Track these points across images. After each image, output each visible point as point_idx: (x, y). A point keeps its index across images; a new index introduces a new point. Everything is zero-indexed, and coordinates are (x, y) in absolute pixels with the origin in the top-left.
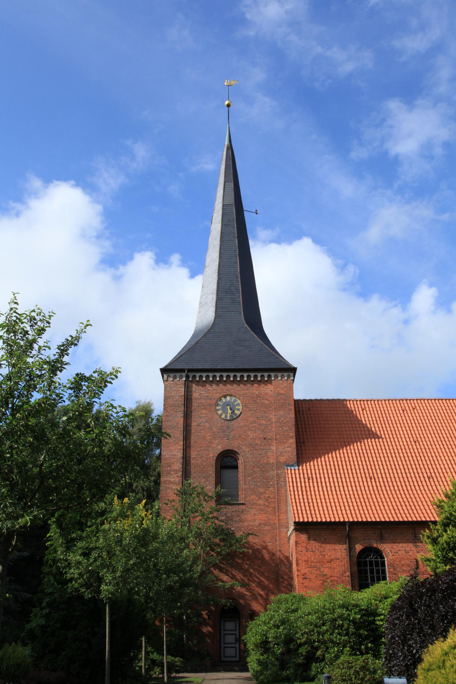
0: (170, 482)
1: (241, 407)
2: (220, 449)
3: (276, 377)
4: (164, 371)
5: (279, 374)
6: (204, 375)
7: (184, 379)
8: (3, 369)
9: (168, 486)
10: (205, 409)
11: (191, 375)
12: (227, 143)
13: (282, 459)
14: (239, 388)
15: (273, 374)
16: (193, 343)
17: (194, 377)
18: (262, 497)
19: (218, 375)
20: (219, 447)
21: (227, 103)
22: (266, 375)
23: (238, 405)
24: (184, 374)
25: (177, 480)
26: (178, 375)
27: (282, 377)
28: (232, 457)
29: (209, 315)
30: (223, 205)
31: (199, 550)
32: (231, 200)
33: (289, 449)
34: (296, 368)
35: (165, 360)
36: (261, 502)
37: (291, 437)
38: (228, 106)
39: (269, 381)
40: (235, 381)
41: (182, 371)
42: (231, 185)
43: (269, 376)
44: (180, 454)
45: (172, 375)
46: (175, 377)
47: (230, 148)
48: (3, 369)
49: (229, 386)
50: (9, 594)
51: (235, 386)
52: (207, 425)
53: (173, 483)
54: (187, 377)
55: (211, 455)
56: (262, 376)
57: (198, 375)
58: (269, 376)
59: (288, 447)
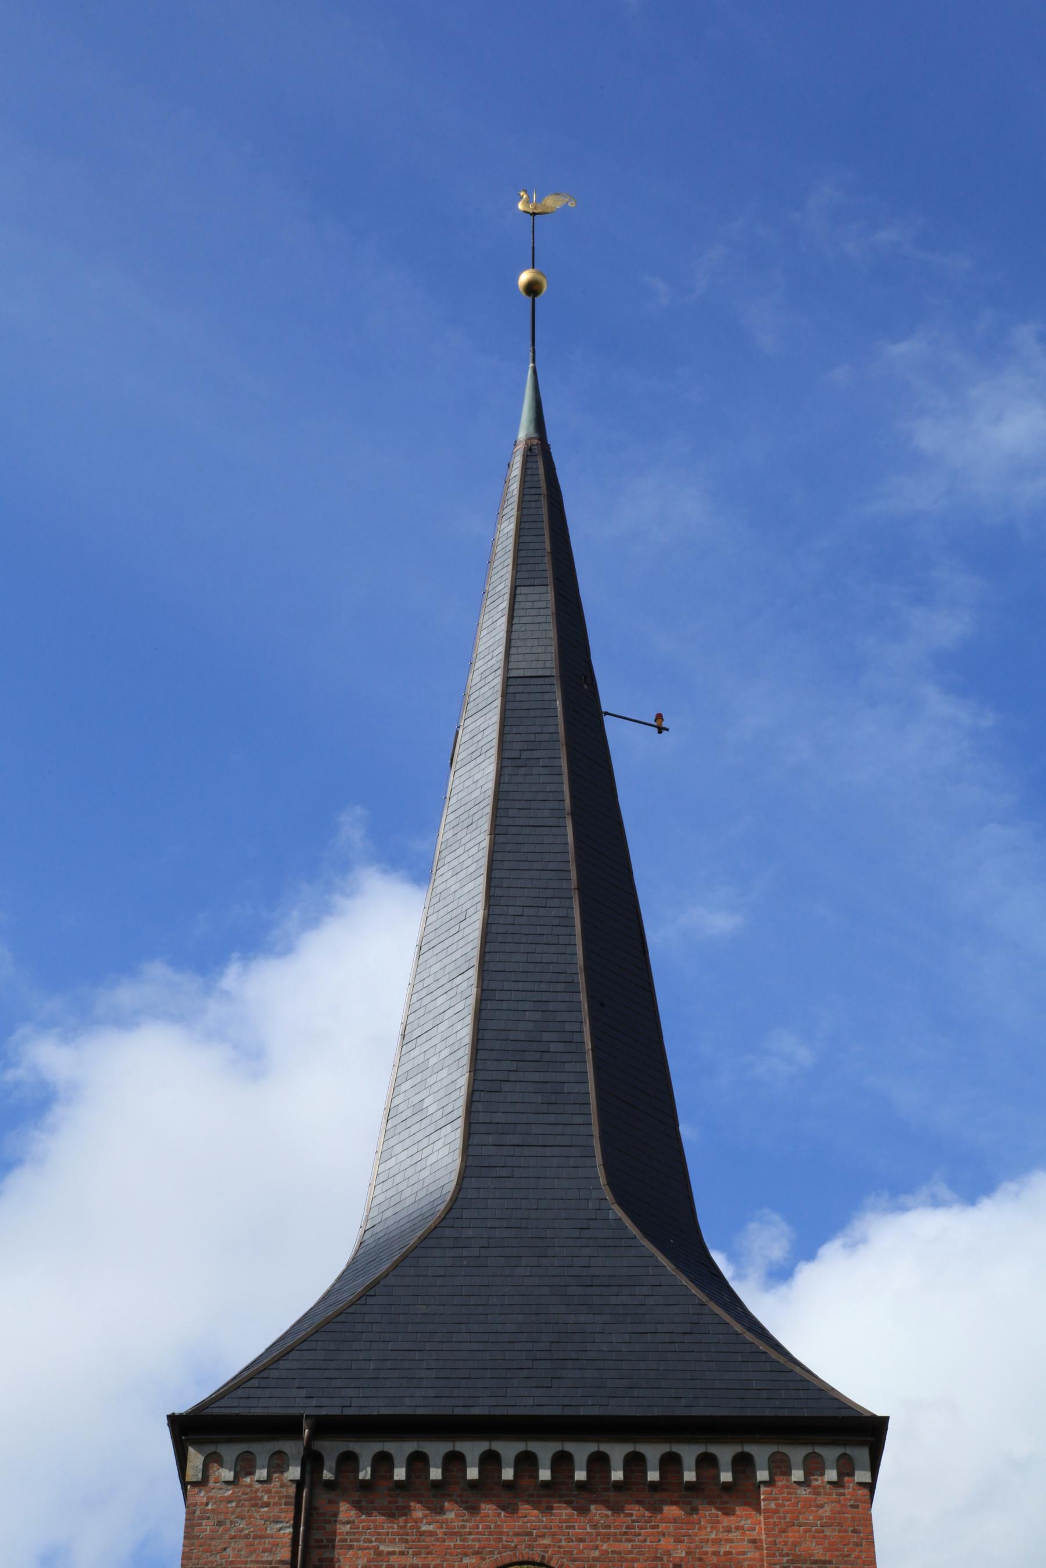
3: (780, 1466)
4: (188, 1429)
5: (797, 1454)
6: (401, 1450)
7: (294, 1472)
11: (331, 1449)
12: (524, 431)
14: (582, 1526)
15: (761, 1453)
16: (348, 1296)
17: (348, 1460)
19: (472, 1450)
21: (525, 277)
22: (725, 1453)
24: (294, 1448)
26: (262, 1450)
27: (813, 1467)
29: (437, 1159)
30: (507, 680)
32: (543, 655)
38: (532, 289)
39: (742, 1492)
40: (559, 1489)
41: (283, 1427)
42: (543, 599)
43: (743, 1464)
45: (230, 1452)
46: (245, 1466)
47: (539, 451)
49: (530, 1515)
51: (563, 1512)
54: (312, 1461)
56: (707, 1462)
57: (366, 1451)
58: (743, 1464)
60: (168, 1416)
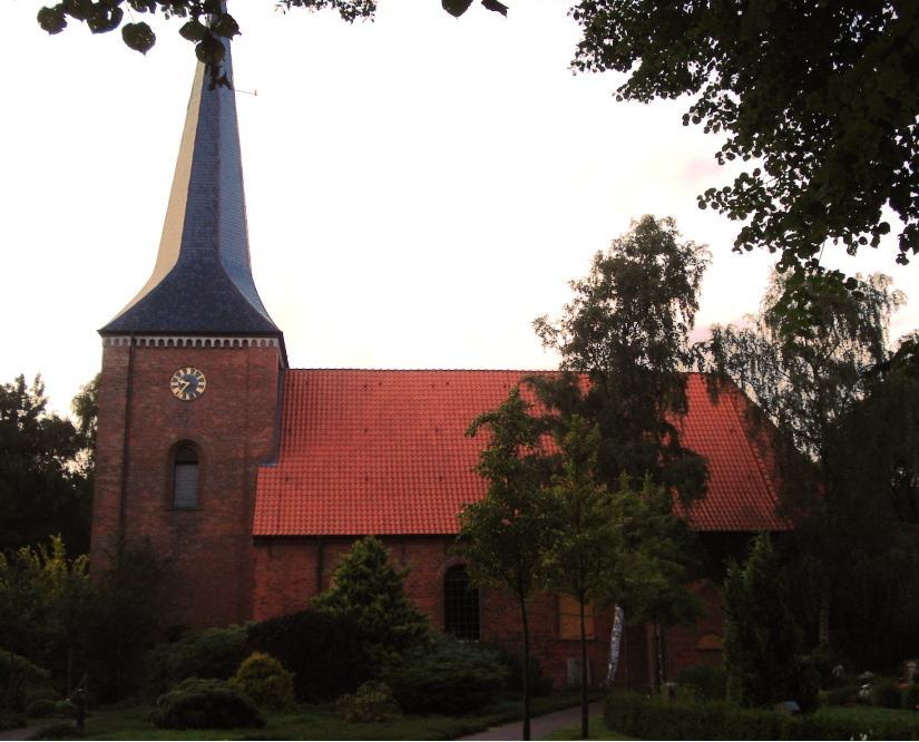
0: (106, 482)
1: (204, 384)
2: (173, 437)
4: (104, 332)
8: (116, 34)
9: (103, 486)
10: (157, 385)
13: (256, 453)
18: (226, 501)
20: (173, 436)
23: (202, 380)
25: (116, 479)
28: (191, 450)
31: (96, 592)
33: (264, 440)
34: (649, 225)
35: (106, 319)
36: (224, 508)
37: (269, 424)
44: (120, 447)
48: (116, 34)
50: (811, 72)
52: (159, 407)
53: (112, 483)
55: (162, 448)
59: (265, 437)
60: (649, 225)
